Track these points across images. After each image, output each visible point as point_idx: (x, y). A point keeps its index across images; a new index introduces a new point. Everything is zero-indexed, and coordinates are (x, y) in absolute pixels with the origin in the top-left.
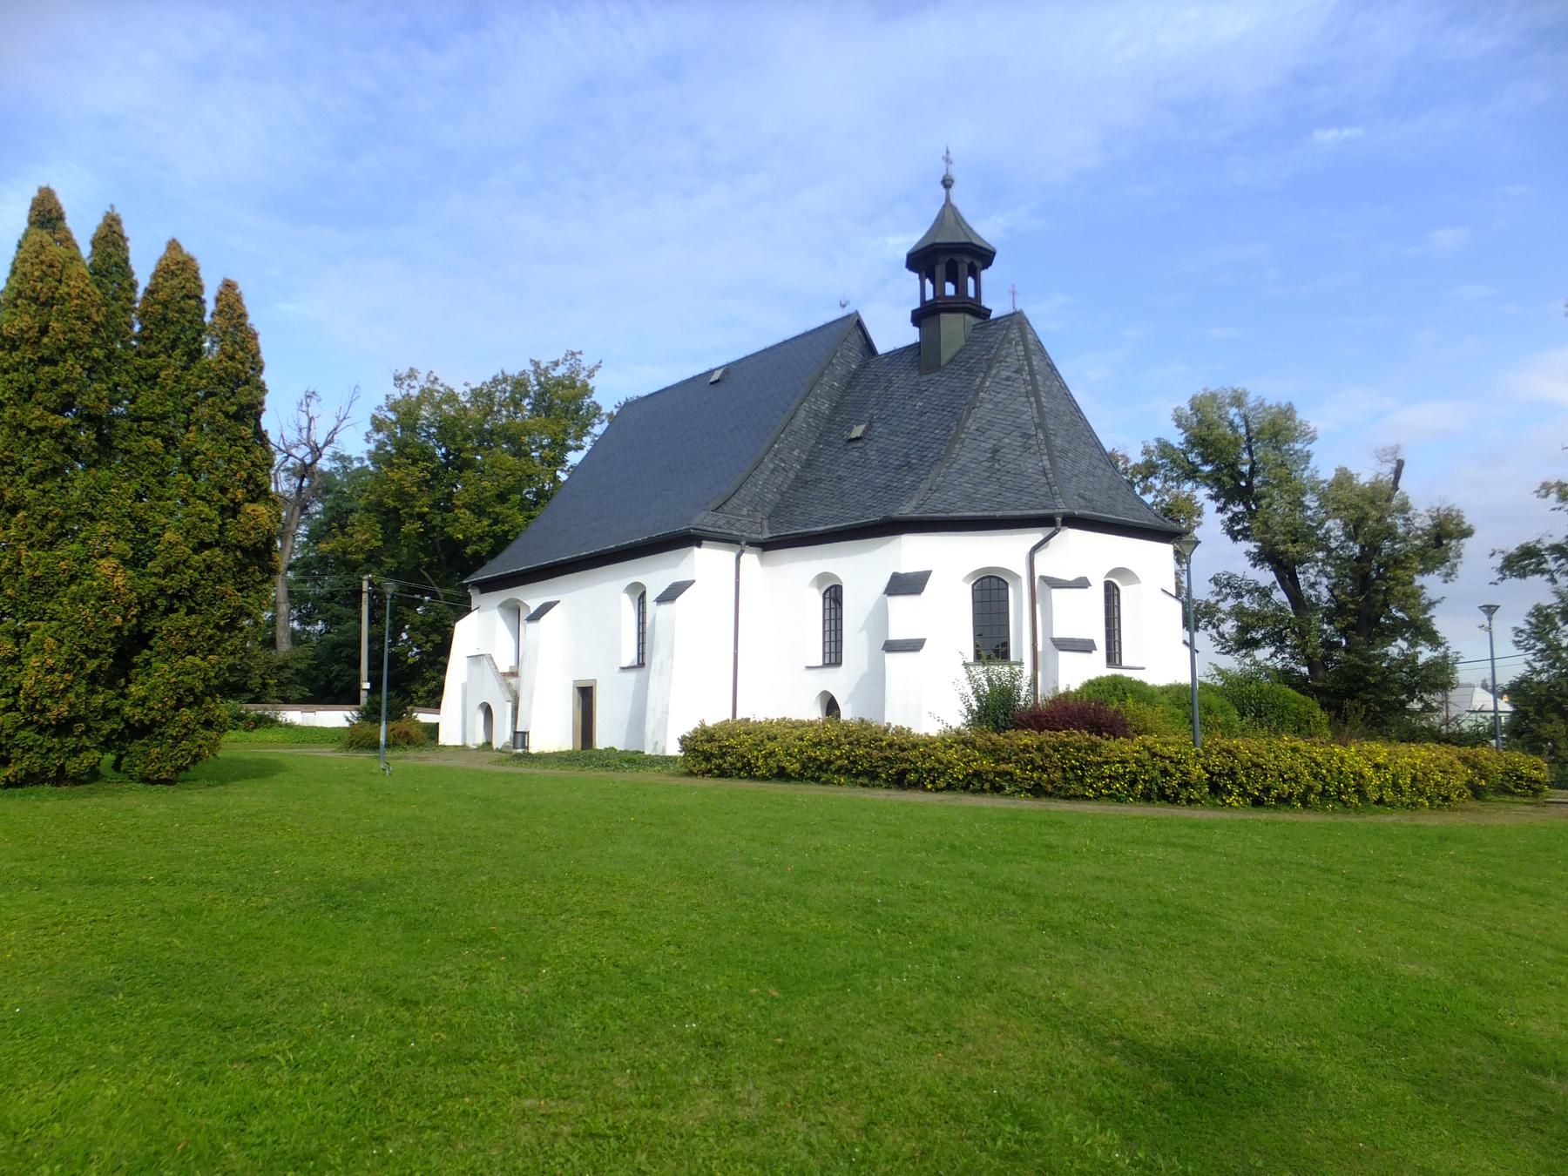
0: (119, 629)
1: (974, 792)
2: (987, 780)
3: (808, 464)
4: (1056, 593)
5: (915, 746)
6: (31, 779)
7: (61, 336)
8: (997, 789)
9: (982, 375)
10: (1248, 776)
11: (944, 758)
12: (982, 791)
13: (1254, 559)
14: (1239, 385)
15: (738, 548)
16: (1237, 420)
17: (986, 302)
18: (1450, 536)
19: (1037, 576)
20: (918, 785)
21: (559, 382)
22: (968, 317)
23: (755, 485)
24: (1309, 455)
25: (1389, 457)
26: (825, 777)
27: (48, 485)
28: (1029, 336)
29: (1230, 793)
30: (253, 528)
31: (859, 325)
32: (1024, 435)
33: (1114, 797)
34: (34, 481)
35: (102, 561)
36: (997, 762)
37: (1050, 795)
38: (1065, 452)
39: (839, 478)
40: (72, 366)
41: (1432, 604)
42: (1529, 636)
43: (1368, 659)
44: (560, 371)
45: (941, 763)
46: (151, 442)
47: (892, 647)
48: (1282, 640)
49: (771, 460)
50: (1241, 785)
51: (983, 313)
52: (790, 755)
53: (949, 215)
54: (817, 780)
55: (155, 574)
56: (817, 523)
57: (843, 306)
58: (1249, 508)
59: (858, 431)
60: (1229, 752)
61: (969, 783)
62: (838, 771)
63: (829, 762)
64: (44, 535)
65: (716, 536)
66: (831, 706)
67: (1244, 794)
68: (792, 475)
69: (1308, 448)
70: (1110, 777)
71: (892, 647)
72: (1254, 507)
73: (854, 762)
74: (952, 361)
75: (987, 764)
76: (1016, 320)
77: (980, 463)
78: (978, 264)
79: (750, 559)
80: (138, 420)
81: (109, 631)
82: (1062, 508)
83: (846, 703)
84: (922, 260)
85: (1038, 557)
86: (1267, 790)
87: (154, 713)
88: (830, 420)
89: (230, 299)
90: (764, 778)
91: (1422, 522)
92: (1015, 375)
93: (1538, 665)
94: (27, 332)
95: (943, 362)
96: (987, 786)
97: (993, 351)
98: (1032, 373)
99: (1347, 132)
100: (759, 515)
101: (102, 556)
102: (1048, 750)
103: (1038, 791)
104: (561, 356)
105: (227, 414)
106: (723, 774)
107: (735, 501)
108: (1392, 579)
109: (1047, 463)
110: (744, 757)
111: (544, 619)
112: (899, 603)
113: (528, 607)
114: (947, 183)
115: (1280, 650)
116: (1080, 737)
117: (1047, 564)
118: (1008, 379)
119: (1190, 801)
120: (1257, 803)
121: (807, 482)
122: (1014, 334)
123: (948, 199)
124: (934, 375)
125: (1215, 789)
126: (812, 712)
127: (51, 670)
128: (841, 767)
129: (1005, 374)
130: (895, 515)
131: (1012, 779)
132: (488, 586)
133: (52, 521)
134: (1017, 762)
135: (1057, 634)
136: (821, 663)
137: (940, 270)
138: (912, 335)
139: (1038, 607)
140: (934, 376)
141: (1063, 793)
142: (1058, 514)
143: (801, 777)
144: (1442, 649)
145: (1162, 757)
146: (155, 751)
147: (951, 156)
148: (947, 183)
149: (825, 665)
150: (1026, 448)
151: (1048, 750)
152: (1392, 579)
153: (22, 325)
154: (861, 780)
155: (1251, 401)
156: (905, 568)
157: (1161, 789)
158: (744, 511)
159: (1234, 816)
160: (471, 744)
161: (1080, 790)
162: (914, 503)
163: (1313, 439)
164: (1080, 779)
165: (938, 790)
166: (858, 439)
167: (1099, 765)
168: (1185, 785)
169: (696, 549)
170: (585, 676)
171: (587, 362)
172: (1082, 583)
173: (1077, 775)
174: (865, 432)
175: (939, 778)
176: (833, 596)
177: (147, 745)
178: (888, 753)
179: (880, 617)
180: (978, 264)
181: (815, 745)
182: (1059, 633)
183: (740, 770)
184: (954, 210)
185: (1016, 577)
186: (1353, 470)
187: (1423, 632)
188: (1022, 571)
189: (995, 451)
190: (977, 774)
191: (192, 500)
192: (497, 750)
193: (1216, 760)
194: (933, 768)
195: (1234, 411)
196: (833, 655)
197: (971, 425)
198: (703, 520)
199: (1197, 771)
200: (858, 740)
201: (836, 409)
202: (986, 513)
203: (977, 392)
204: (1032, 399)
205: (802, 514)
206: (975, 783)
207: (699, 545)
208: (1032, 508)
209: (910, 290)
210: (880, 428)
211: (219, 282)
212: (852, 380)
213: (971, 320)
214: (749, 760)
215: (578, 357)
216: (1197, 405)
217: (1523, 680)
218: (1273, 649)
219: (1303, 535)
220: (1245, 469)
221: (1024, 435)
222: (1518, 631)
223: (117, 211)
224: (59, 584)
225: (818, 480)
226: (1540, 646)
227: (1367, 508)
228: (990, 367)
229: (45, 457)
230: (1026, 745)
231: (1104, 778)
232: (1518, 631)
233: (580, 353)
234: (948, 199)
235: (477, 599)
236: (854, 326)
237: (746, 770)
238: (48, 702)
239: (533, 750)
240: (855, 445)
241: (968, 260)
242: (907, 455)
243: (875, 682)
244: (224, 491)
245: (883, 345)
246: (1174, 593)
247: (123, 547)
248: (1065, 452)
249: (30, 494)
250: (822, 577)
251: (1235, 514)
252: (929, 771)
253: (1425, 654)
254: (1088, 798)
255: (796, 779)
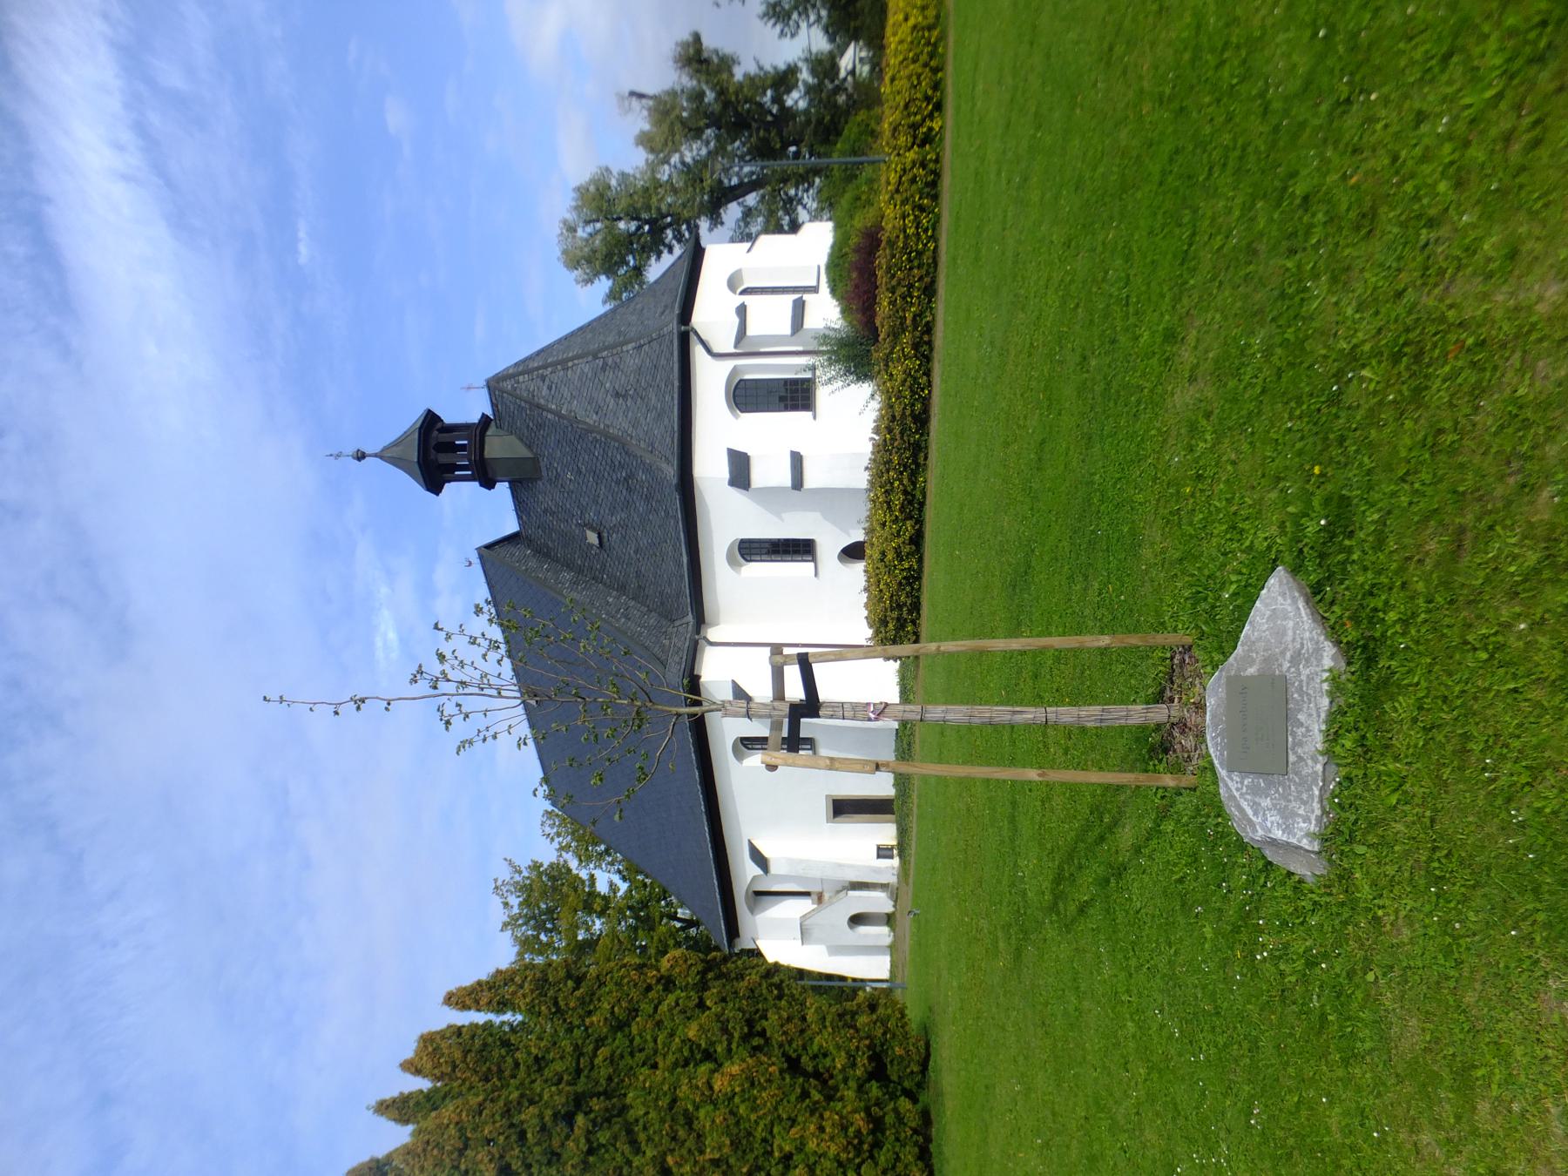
0: (781, 1071)
1: (931, 350)
2: (921, 338)
3: (622, 589)
4: (751, 331)
5: (891, 407)
6: (924, 1155)
7: (498, 1125)
8: (929, 329)
9: (545, 413)
10: (916, 114)
11: (900, 377)
12: (930, 343)
13: (715, 225)
14: (556, 229)
15: (702, 642)
16: (589, 229)
17: (474, 418)
18: (699, 51)
19: (733, 350)
20: (926, 402)
21: (526, 903)
22: (489, 433)
23: (641, 634)
24: (623, 175)
25: (626, 103)
26: (919, 496)
27: (642, 1137)
28: (511, 371)
29: (931, 129)
30: (686, 961)
31: (489, 547)
32: (603, 369)
33: (935, 226)
34: (637, 1150)
35: (716, 1088)
36: (904, 331)
37: (933, 282)
38: (620, 333)
39: (636, 552)
40: (529, 1115)
41: (761, 68)
42: (788, 25)
43: (808, 122)
44: (514, 901)
45: (905, 380)
46: (600, 1058)
47: (798, 482)
48: (791, 200)
49: (618, 620)
50: (924, 120)
51: (485, 421)
52: (899, 531)
53: (389, 455)
54: (922, 504)
55: (730, 1044)
56: (680, 565)
57: (470, 564)
58: (670, 225)
59: (592, 538)
60: (895, 129)
61: (923, 355)
62: (914, 484)
63: (905, 492)
64: (690, 1143)
65: (690, 662)
66: (853, 552)
67: (931, 116)
68: (632, 603)
69: (615, 173)
70: (917, 228)
71: (798, 482)
72: (669, 219)
73: (905, 467)
74: (529, 447)
75: (906, 338)
76: (495, 387)
77: (628, 409)
78: (439, 425)
79: (713, 634)
80: (578, 1071)
81: (784, 1079)
82: (673, 326)
83: (849, 535)
84: (434, 479)
85: (716, 350)
86: (928, 99)
87: (861, 1045)
88: (580, 571)
89: (460, 999)
90: (920, 561)
91: (687, 81)
92: (547, 382)
93: (812, 18)
94: (493, 1156)
95: (530, 455)
96: (926, 338)
97: (523, 404)
98: (545, 367)
99: (302, 234)
100: (670, 629)
101: (711, 1088)
102: (894, 282)
103: (930, 291)
104: (498, 901)
105: (575, 989)
106: (916, 607)
107: (656, 650)
108: (737, 96)
109: (630, 346)
110: (900, 583)
111: (766, 854)
112: (758, 477)
113: (754, 878)
114: (361, 456)
115: (800, 201)
116: (882, 259)
117: (724, 341)
118: (550, 388)
119: (937, 161)
120: (939, 107)
121: (640, 587)
122: (508, 385)
123: (376, 455)
124: (542, 464)
125: (927, 139)
126: (857, 572)
127: (822, 1129)
128: (910, 480)
129: (545, 391)
130: (675, 481)
131: (920, 315)
132: (733, 930)
133: (677, 1131)
134: (904, 310)
135: (788, 331)
136: (812, 564)
137: (444, 458)
138: (503, 489)
139: (762, 350)
140: (543, 463)
141: (932, 270)
142: (678, 328)
143: (920, 522)
144: (800, 64)
145: (900, 183)
146: (898, 1051)
147: (335, 453)
148: (361, 456)
149: (814, 560)
150: (616, 366)
151: (894, 282)
152: (737, 96)
153: (486, 1160)
154: (921, 461)
155: (570, 216)
156: (723, 470)
157: (927, 184)
158: (666, 642)
159: (949, 124)
160: (888, 940)
161: (929, 254)
162: (664, 466)
163: (607, 169)
164: (920, 254)
165: (930, 384)
166: (600, 537)
167: (907, 237)
168: (923, 165)
169: (702, 680)
170: (823, 808)
171: (505, 874)
172: (742, 311)
173: (915, 258)
174: (593, 529)
175: (920, 384)
176: (751, 550)
177: (892, 1062)
178: (897, 431)
179: (769, 496)
180: (439, 425)
181: (889, 507)
182: (786, 329)
183: (913, 589)
184: (385, 449)
185: (735, 370)
186: (636, 131)
187: (784, 80)
188: (729, 365)
189: (617, 395)
190: (916, 346)
191: (657, 1017)
192: (895, 906)
193: (902, 140)
194: (910, 387)
195: (580, 233)
196: (800, 549)
197: (592, 419)
198: (674, 674)
199: (911, 155)
200: (885, 463)
201: (569, 566)
202: (676, 396)
203: (561, 416)
204: (570, 364)
205: (670, 584)
206: (923, 350)
207: (699, 677)
208: (672, 354)
209: (461, 493)
210: (591, 515)
211: (446, 1008)
212: (543, 553)
213: (492, 430)
214: (904, 578)
215: (499, 883)
216: (573, 262)
217: (826, 30)
218: (800, 208)
219: (693, 173)
220: (633, 226)
221: (603, 369)
222: (782, 35)
223: (373, 1103)
224: (737, 1123)
225: (638, 574)
226: (795, 16)
227: (673, 116)
228: (538, 406)
229: (615, 1138)
230: (890, 303)
231: (918, 234)
232: (782, 35)
233: (496, 880)
234: (376, 455)
235: (744, 943)
236: (489, 552)
237: (913, 579)
238: (851, 1130)
239: (894, 843)
240: (605, 540)
241: (435, 433)
242: (618, 482)
243: (829, 498)
244: (649, 988)
245: (511, 526)
246: (749, 244)
247: (704, 1068)
248: (620, 333)
249: (650, 1153)
250: (731, 561)
251: (675, 237)
252: (913, 393)
253: (805, 75)
254: (936, 248)
255: (921, 527)
